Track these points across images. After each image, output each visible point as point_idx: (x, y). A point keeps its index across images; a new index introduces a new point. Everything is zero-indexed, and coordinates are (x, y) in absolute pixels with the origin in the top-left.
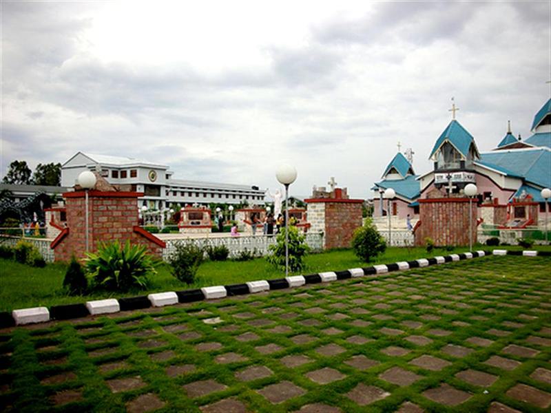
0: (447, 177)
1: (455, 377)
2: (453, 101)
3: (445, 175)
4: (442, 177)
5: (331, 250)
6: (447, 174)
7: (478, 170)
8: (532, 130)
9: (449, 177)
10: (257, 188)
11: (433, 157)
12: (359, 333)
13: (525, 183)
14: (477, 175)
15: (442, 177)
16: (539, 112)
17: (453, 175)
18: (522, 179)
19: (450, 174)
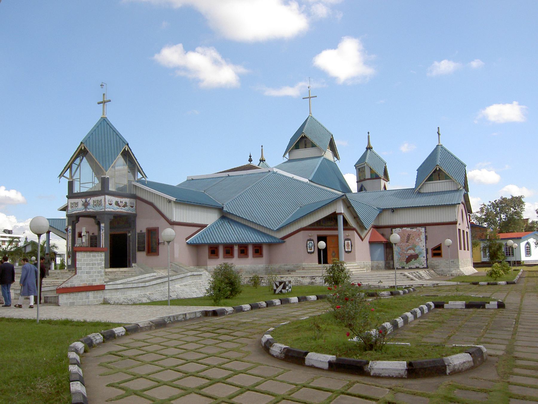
0: (83, 205)
1: (376, 343)
2: (493, 304)
3: (80, 201)
4: (77, 204)
5: (15, 299)
6: (84, 200)
7: (140, 194)
8: (284, 156)
9: (86, 205)
10: (10, 232)
11: (67, 174)
12: (142, 377)
13: (225, 216)
14: (138, 201)
15: (77, 204)
16: (302, 125)
17: (91, 200)
18: (220, 209)
19: (88, 199)
